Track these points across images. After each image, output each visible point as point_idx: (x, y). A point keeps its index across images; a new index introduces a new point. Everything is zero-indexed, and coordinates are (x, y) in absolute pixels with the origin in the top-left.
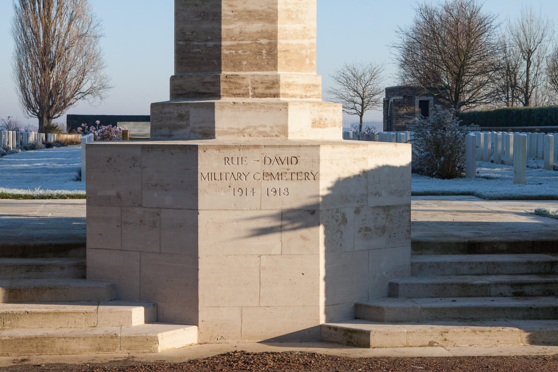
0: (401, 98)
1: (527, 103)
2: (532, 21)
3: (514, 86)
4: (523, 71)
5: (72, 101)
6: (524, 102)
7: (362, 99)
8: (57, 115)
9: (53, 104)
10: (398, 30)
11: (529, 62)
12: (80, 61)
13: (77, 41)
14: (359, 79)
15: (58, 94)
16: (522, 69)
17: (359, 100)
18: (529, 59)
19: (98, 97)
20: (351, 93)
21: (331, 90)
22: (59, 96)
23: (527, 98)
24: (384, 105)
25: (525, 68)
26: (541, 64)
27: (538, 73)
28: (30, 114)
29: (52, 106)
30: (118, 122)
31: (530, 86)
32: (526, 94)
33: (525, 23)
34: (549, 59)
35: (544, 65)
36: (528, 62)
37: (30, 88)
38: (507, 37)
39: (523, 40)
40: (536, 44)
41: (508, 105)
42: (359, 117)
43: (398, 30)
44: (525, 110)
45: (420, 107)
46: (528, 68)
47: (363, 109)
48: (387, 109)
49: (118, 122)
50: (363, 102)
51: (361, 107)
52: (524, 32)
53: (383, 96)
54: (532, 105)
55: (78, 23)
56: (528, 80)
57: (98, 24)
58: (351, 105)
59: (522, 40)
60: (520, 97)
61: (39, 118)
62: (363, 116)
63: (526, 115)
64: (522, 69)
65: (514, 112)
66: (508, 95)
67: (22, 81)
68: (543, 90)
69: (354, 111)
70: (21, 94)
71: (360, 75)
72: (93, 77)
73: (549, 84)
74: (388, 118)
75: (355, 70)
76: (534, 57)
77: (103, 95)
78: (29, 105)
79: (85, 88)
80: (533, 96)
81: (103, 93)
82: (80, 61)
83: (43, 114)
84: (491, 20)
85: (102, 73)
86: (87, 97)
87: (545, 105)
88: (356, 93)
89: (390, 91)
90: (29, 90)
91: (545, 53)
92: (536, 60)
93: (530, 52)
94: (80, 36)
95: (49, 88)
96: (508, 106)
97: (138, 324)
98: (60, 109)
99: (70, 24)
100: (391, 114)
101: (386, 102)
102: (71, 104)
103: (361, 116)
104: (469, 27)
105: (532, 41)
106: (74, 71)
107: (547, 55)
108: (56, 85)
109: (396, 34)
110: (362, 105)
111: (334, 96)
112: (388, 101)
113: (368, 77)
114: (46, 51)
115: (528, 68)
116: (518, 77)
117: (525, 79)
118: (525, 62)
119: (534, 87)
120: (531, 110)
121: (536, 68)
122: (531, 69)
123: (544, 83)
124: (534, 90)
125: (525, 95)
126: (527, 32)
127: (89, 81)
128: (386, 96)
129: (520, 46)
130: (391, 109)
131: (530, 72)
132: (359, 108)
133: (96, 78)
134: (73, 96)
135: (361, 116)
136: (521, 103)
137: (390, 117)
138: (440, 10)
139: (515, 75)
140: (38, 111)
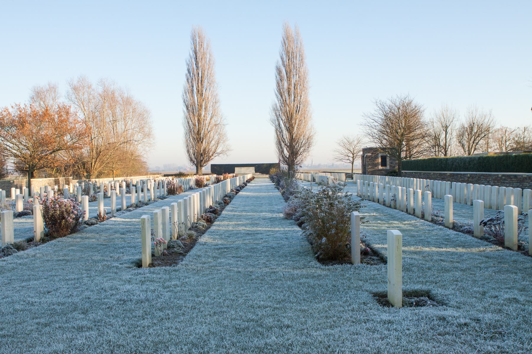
0: (370, 154)
1: (445, 155)
2: (447, 110)
3: (439, 145)
4: (443, 137)
5: (212, 157)
6: (444, 154)
7: (353, 154)
8: (205, 165)
9: (203, 159)
10: (363, 115)
11: (446, 132)
12: (216, 137)
13: (214, 127)
14: (350, 144)
15: (205, 154)
16: (443, 136)
17: (352, 155)
18: (446, 130)
19: (226, 155)
20: (347, 151)
21: (336, 150)
22: (206, 155)
23: (446, 152)
24: (362, 158)
25: (444, 136)
26: (453, 133)
27: (451, 138)
28: (192, 164)
29: (202, 160)
30: (235, 168)
31: (447, 145)
32: (445, 150)
33: (444, 112)
34: (457, 131)
35: (455, 134)
36: (446, 132)
37: (191, 151)
38: (435, 119)
39: (443, 120)
40: (450, 123)
41: (436, 155)
42: (351, 164)
43: (363, 115)
44: (444, 158)
45: (382, 159)
46: (446, 136)
47: (353, 160)
48: (363, 161)
49: (235, 168)
50: (353, 156)
51: (352, 159)
52: (443, 116)
53: (361, 153)
54: (448, 156)
55: (215, 118)
56: (446, 142)
57: (225, 118)
58: (347, 158)
59: (442, 121)
60: (442, 151)
61: (196, 166)
62: (354, 164)
63: (444, 162)
64: (443, 136)
65: (438, 160)
66: (436, 150)
67: (188, 148)
68: (455, 146)
69: (348, 161)
70: (187, 155)
71: (351, 141)
72: (223, 145)
73: (457, 144)
74: (364, 165)
75: (304, 136)
76: (449, 130)
77: (228, 154)
78: (191, 160)
79: (218, 151)
80: (449, 150)
81: (228, 153)
82: (216, 137)
83: (198, 164)
84: (419, 107)
85: (227, 143)
86: (220, 155)
87: (456, 156)
88: (349, 151)
89: (365, 150)
90: (191, 152)
91: (455, 127)
92: (450, 131)
93: (447, 127)
94: (216, 125)
95: (201, 151)
96: (436, 156)
97: (354, 214)
98: (207, 161)
99: (211, 119)
100: (365, 163)
101: (363, 157)
102: (212, 159)
103: (353, 164)
104: (406, 112)
105: (448, 121)
106: (213, 142)
107: (456, 128)
108: (204, 150)
109: (363, 117)
110: (353, 158)
111: (338, 153)
112: (364, 156)
113: (356, 142)
114: (199, 133)
115: (446, 136)
116: (441, 140)
117: (445, 142)
118: (444, 132)
119: (449, 145)
120: (447, 159)
121: (450, 135)
122: (447, 136)
123: (455, 143)
124: (450, 147)
125: (445, 150)
126: (445, 117)
127: (221, 147)
128: (363, 153)
129: (442, 124)
130: (365, 161)
131: (447, 138)
132: (351, 159)
133: (224, 145)
134: (212, 155)
135: (353, 164)
136: (443, 154)
137: (365, 165)
138: (389, 103)
139: (439, 139)
140: (195, 163)
